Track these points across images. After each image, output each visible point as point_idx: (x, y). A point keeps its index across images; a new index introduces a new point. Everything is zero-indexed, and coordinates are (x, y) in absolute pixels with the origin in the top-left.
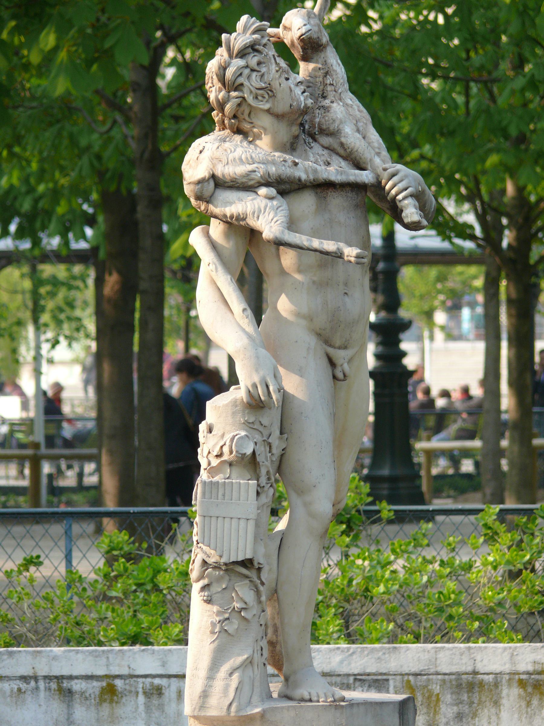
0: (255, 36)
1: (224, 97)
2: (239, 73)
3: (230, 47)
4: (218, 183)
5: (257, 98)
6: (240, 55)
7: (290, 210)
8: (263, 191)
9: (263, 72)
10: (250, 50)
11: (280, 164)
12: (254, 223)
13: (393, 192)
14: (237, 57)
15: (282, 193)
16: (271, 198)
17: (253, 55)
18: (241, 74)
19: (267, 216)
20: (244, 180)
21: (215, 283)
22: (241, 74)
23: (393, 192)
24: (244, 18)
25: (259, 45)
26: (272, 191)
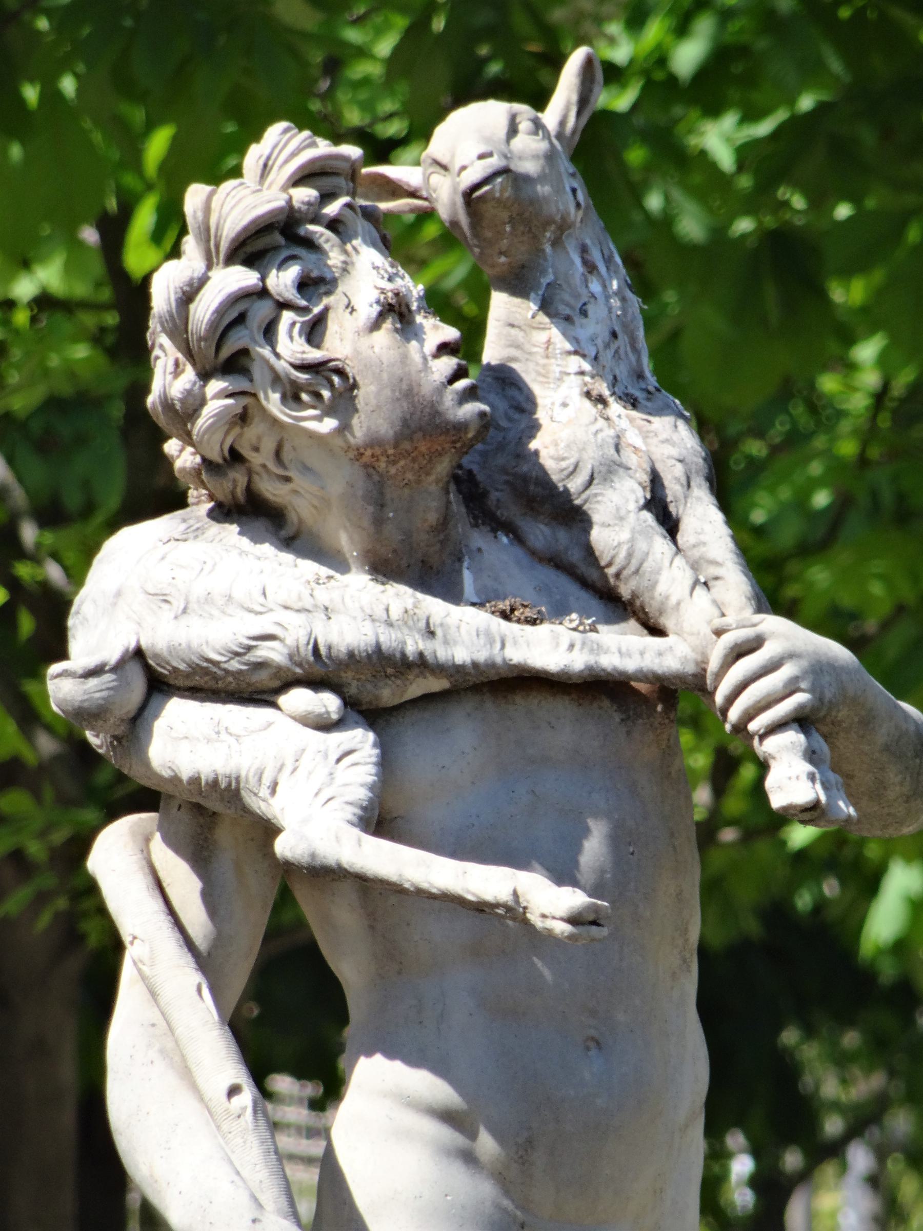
0: (304, 195)
1: (189, 392)
2: (234, 314)
3: (208, 229)
4: (157, 679)
5: (297, 398)
6: (242, 255)
7: (386, 763)
8: (299, 699)
9: (624, 460)
10: (279, 239)
11: (360, 610)
12: (263, 805)
13: (734, 714)
14: (230, 260)
15: (362, 711)
16: (325, 725)
17: (285, 253)
18: (241, 319)
19: (311, 786)
20: (235, 665)
21: (231, 1163)
22: (241, 319)
23: (734, 714)
24: (275, 132)
25: (315, 220)
26: (329, 703)
